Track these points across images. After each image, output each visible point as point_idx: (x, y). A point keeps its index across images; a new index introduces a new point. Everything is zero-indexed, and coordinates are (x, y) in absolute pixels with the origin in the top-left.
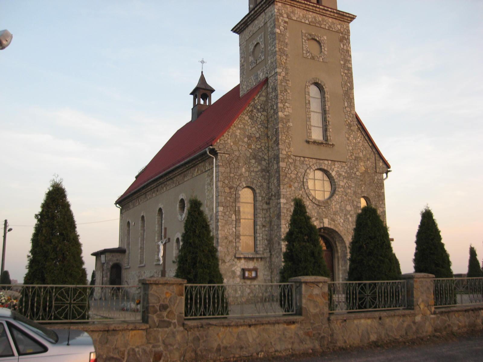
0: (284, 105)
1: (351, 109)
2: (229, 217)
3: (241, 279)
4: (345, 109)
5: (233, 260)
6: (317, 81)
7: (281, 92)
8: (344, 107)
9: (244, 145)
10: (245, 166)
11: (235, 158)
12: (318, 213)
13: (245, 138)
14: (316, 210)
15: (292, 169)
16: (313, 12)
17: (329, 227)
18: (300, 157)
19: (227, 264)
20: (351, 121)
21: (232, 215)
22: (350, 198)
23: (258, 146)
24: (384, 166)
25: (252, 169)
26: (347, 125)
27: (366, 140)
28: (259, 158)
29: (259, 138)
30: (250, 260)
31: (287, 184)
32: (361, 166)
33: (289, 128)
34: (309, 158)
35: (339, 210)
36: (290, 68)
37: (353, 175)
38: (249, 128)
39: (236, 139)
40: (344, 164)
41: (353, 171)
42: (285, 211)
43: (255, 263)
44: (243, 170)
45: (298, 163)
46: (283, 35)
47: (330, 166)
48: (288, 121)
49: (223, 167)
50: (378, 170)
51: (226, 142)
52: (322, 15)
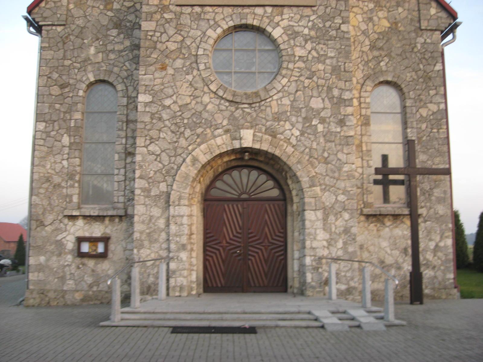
2: (56, 140)
3: (74, 257)
5: (61, 222)
9: (98, 5)
10: (96, 44)
11: (76, 30)
12: (232, 118)
14: (227, 114)
15: (171, 31)
17: (257, 146)
19: (49, 229)
21: (63, 135)
22: (321, 82)
24: (443, 14)
25: (110, 47)
28: (128, 24)
30: (97, 221)
31: (155, 63)
32: (379, 18)
35: (289, 109)
37: (334, 33)
40: (307, 11)
42: (147, 119)
43: (106, 227)
44: (92, 50)
45: (186, 20)
47: (267, 17)
49: (51, 50)
50: (424, 25)
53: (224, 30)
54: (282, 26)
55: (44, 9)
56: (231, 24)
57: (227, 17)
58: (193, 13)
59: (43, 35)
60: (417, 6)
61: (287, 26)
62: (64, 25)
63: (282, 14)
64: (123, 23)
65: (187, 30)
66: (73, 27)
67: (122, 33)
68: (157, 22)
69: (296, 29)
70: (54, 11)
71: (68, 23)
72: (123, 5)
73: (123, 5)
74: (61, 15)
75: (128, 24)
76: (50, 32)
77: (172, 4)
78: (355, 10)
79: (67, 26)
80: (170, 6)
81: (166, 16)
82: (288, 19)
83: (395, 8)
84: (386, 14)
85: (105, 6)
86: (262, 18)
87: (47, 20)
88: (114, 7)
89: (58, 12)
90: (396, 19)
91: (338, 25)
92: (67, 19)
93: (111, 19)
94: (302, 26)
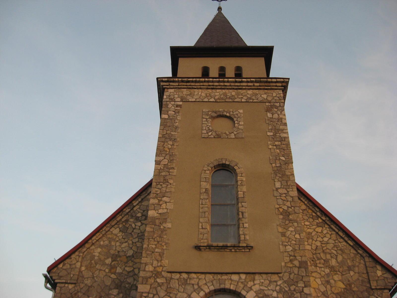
0: (159, 201)
1: (288, 190)
4: (275, 192)
6: (224, 162)
7: (157, 185)
8: (274, 189)
13: (108, 258)
16: (221, 89)
18: (180, 273)
20: (288, 207)
23: (128, 269)
26: (281, 214)
27: (342, 237)
28: (127, 286)
29: (133, 256)
32: (335, 281)
33: (164, 230)
34: (198, 273)
36: (177, 153)
38: (118, 244)
39: (91, 261)
40: (275, 277)
41: (297, 286)
45: (175, 284)
46: (171, 119)
47: (242, 283)
48: (165, 220)
51: (73, 266)
52: (236, 89)
53: (206, 294)
54: (255, 290)
55: (62, 269)
56: (212, 288)
57: (208, 282)
58: (181, 278)
59: (56, 290)
60: (365, 269)
61: (259, 290)
62: (75, 284)
63: (254, 280)
64: (123, 285)
65: (176, 293)
66: (82, 285)
67: (122, 293)
68: (151, 285)
69: (266, 292)
70: (69, 272)
71: (79, 282)
72: (124, 269)
73: (124, 269)
74: (74, 275)
75: (127, 286)
76: (63, 288)
77: (164, 271)
78: (314, 274)
79: (77, 285)
80: (163, 273)
81: (159, 280)
82: (259, 284)
83: (347, 272)
84: (340, 278)
85: (110, 271)
86: (238, 283)
87: (62, 278)
88: (117, 271)
89: (72, 273)
90: (349, 281)
91: (301, 289)
92: (78, 279)
93: (113, 281)
94: (272, 290)
